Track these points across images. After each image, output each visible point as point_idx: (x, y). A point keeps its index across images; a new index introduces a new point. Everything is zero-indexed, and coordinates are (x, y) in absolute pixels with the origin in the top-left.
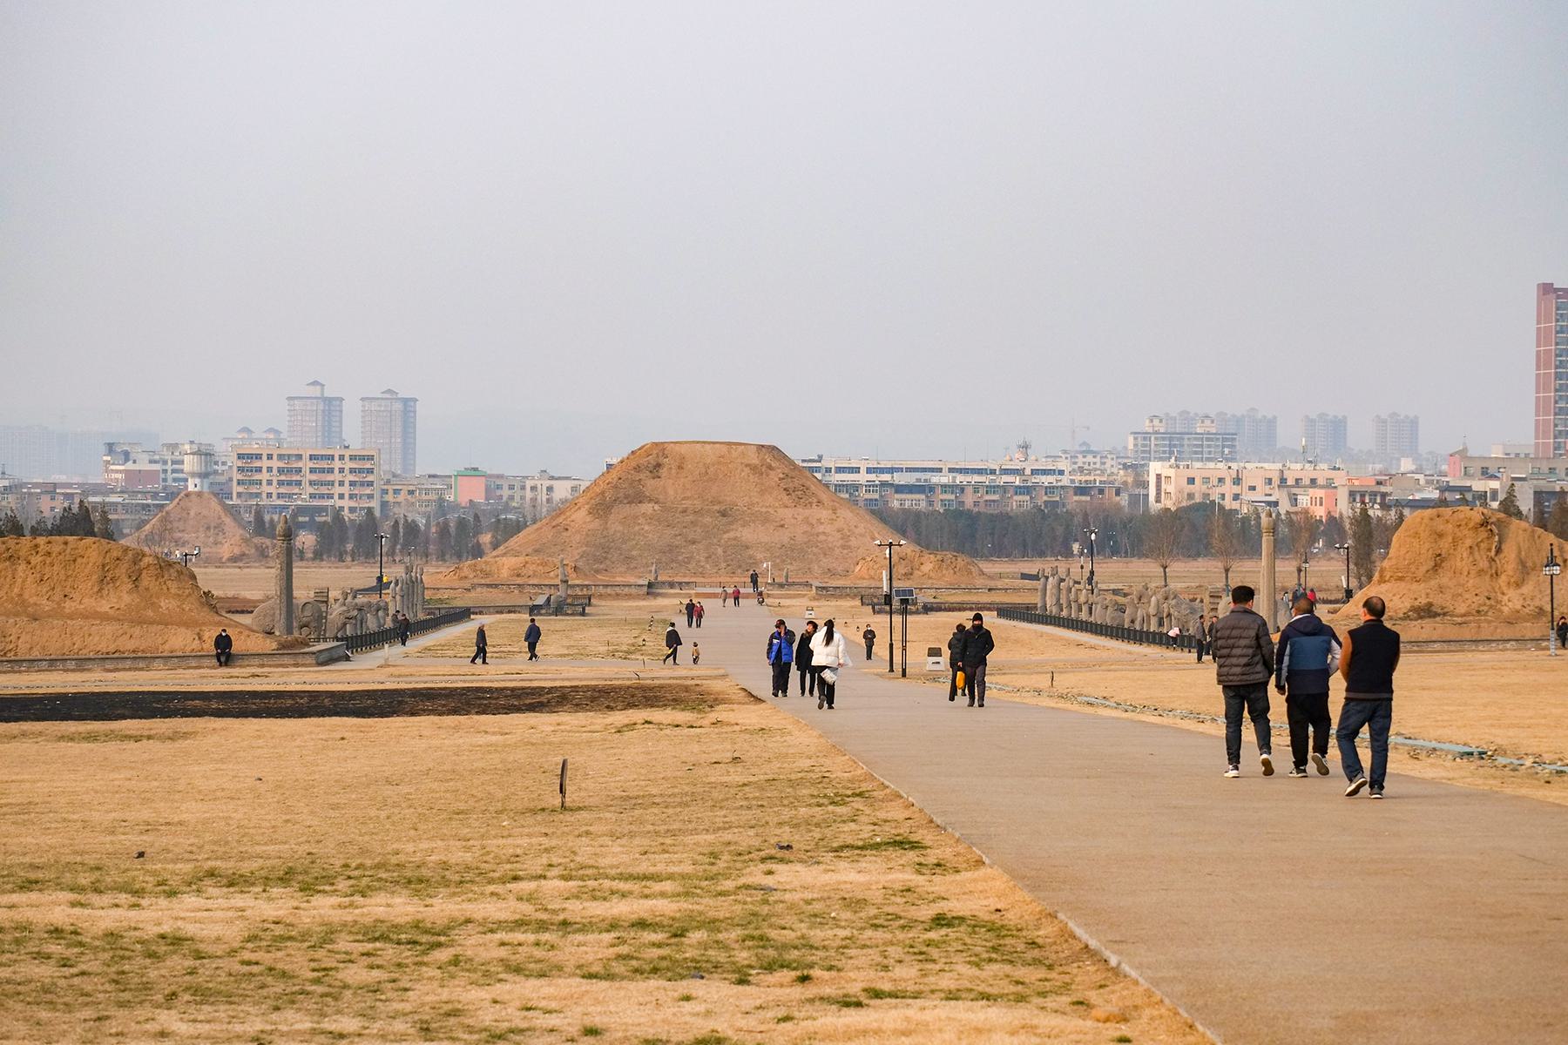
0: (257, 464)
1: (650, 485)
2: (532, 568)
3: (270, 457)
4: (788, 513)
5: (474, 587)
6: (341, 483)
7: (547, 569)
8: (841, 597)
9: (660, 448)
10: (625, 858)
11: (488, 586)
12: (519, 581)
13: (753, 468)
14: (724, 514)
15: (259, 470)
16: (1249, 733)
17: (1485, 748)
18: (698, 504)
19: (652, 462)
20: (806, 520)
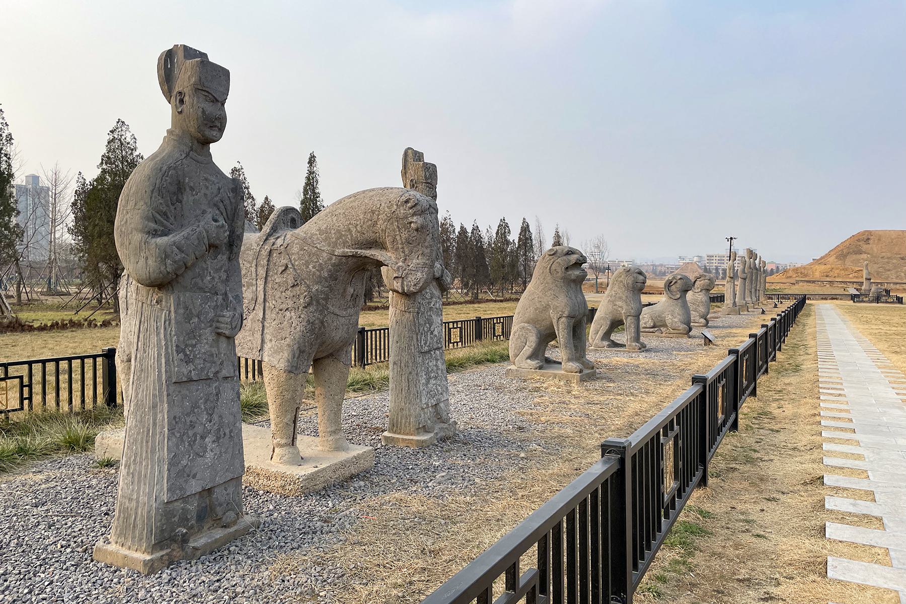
1: (865, 247)
5: (797, 282)
7: (847, 273)
10: (279, 242)
11: (808, 282)
17: (258, 471)
18: (889, 255)
19: (866, 238)
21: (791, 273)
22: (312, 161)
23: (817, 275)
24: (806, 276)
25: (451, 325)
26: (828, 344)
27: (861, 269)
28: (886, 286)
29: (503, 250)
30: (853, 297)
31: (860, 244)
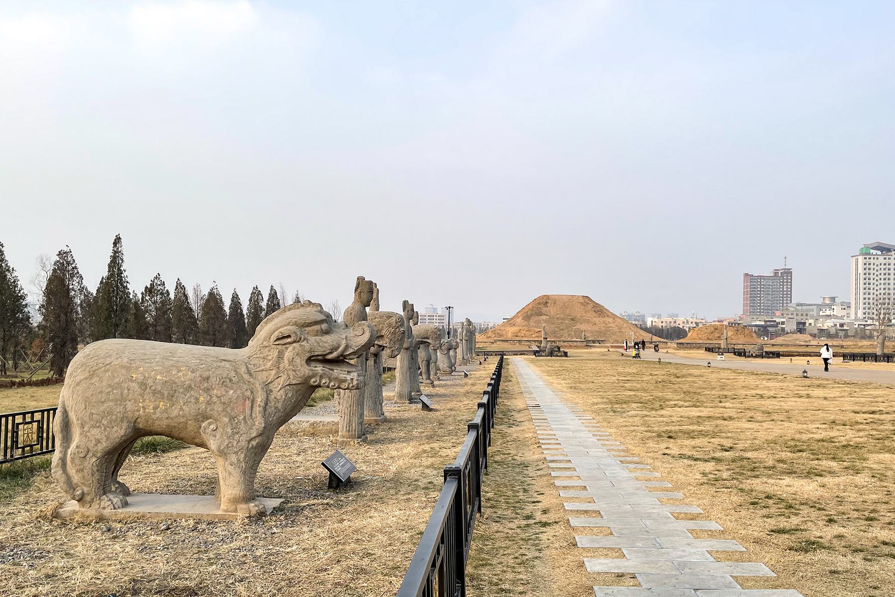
1: (544, 309)
2: (524, 332)
4: (597, 319)
5: (496, 341)
8: (690, 348)
9: (548, 296)
12: (517, 339)
13: (582, 304)
14: (572, 320)
16: (605, 400)
18: (562, 316)
20: (604, 322)
21: (490, 334)
22: (117, 241)
23: (509, 336)
24: (501, 336)
25: (19, 419)
26: (521, 375)
27: (539, 330)
28: (558, 344)
29: (18, 300)
30: (535, 353)
31: (540, 307)
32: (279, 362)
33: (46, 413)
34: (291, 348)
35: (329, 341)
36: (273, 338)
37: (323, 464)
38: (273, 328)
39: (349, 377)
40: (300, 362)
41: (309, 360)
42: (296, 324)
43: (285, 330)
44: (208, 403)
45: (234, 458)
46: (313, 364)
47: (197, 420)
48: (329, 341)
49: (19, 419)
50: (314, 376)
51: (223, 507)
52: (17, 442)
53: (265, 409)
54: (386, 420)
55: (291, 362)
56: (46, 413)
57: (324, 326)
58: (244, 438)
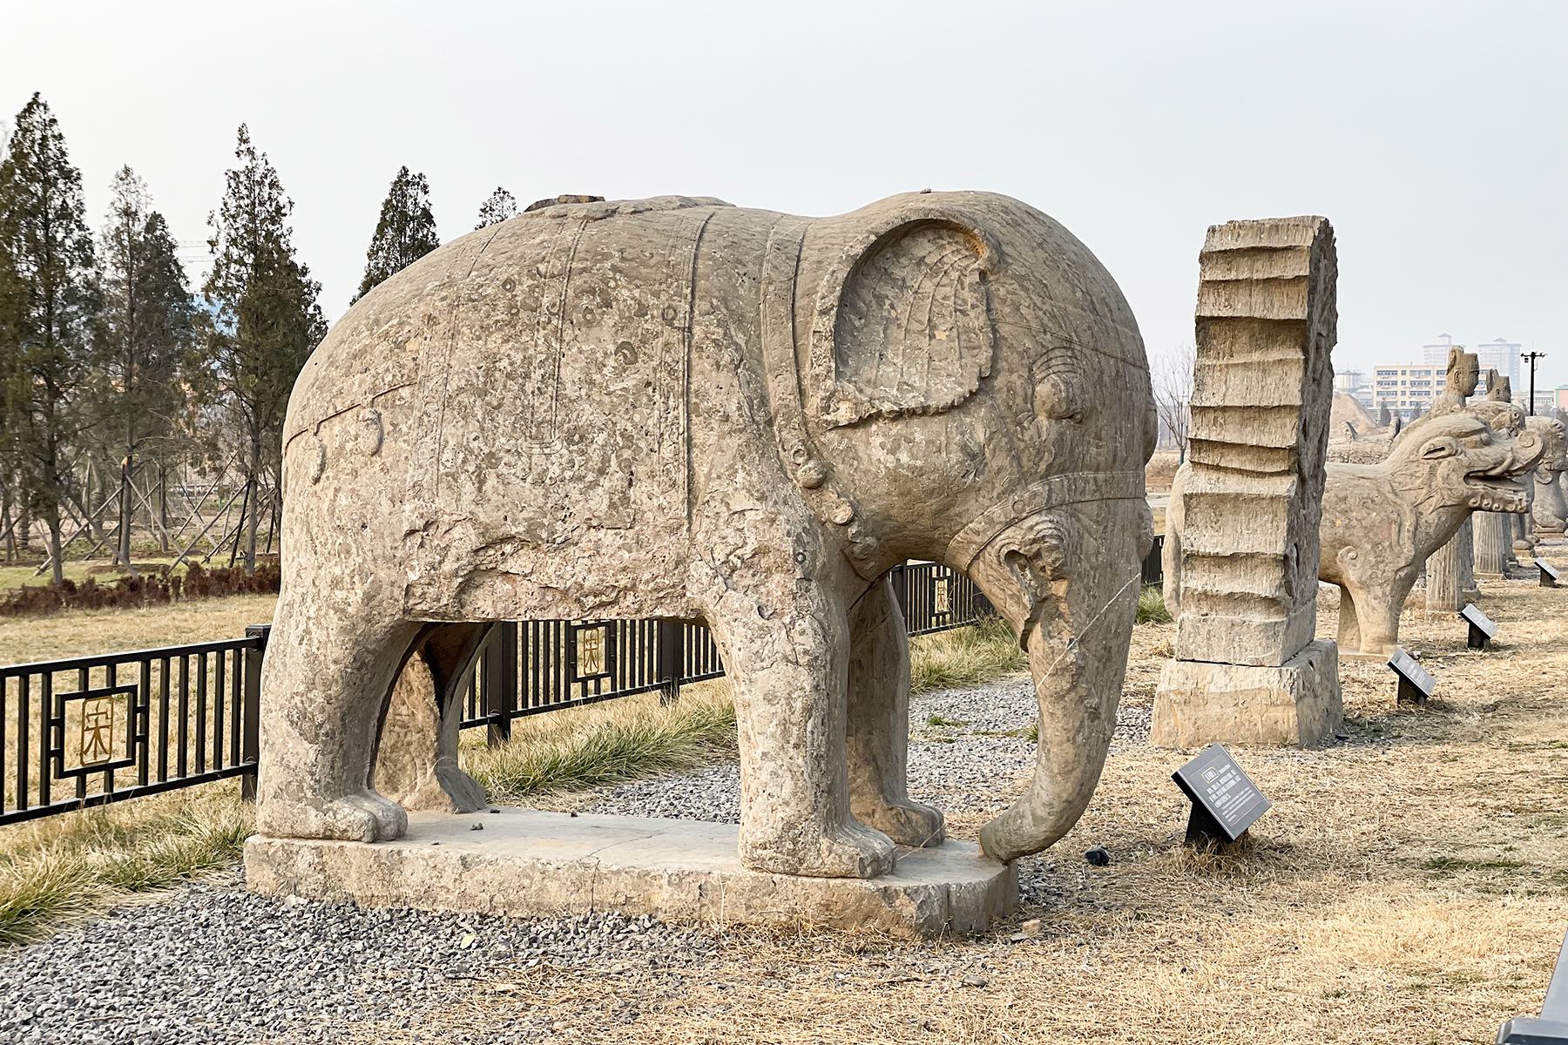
0: (1394, 378)
3: (1404, 373)
6: (1403, 393)
15: (1395, 383)
32: (1430, 480)
33: (212, 655)
34: (1445, 462)
35: (1491, 453)
36: (1422, 451)
37: (1176, 777)
38: (1421, 439)
39: (1516, 498)
40: (1456, 479)
41: (1467, 477)
42: (1449, 434)
43: (1438, 441)
44: (1347, 527)
45: (1378, 591)
46: (1472, 482)
47: (1333, 547)
48: (1491, 453)
49: (64, 682)
50: (1472, 496)
51: (1363, 647)
52: (60, 754)
53: (1415, 535)
54: (1480, 596)
55: (1446, 478)
56: (156, 663)
57: (1484, 436)
58: (1390, 568)
